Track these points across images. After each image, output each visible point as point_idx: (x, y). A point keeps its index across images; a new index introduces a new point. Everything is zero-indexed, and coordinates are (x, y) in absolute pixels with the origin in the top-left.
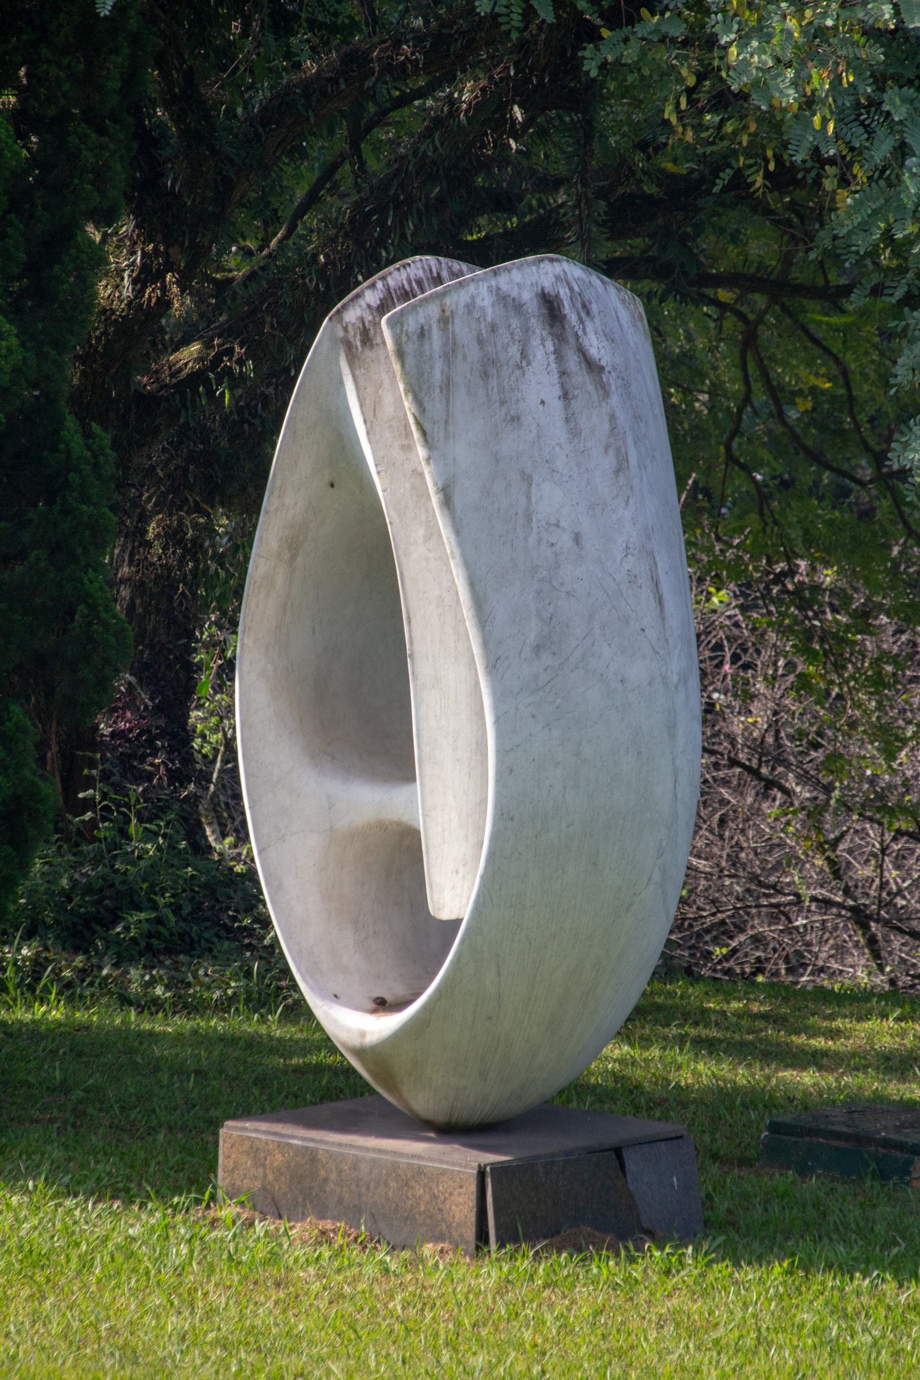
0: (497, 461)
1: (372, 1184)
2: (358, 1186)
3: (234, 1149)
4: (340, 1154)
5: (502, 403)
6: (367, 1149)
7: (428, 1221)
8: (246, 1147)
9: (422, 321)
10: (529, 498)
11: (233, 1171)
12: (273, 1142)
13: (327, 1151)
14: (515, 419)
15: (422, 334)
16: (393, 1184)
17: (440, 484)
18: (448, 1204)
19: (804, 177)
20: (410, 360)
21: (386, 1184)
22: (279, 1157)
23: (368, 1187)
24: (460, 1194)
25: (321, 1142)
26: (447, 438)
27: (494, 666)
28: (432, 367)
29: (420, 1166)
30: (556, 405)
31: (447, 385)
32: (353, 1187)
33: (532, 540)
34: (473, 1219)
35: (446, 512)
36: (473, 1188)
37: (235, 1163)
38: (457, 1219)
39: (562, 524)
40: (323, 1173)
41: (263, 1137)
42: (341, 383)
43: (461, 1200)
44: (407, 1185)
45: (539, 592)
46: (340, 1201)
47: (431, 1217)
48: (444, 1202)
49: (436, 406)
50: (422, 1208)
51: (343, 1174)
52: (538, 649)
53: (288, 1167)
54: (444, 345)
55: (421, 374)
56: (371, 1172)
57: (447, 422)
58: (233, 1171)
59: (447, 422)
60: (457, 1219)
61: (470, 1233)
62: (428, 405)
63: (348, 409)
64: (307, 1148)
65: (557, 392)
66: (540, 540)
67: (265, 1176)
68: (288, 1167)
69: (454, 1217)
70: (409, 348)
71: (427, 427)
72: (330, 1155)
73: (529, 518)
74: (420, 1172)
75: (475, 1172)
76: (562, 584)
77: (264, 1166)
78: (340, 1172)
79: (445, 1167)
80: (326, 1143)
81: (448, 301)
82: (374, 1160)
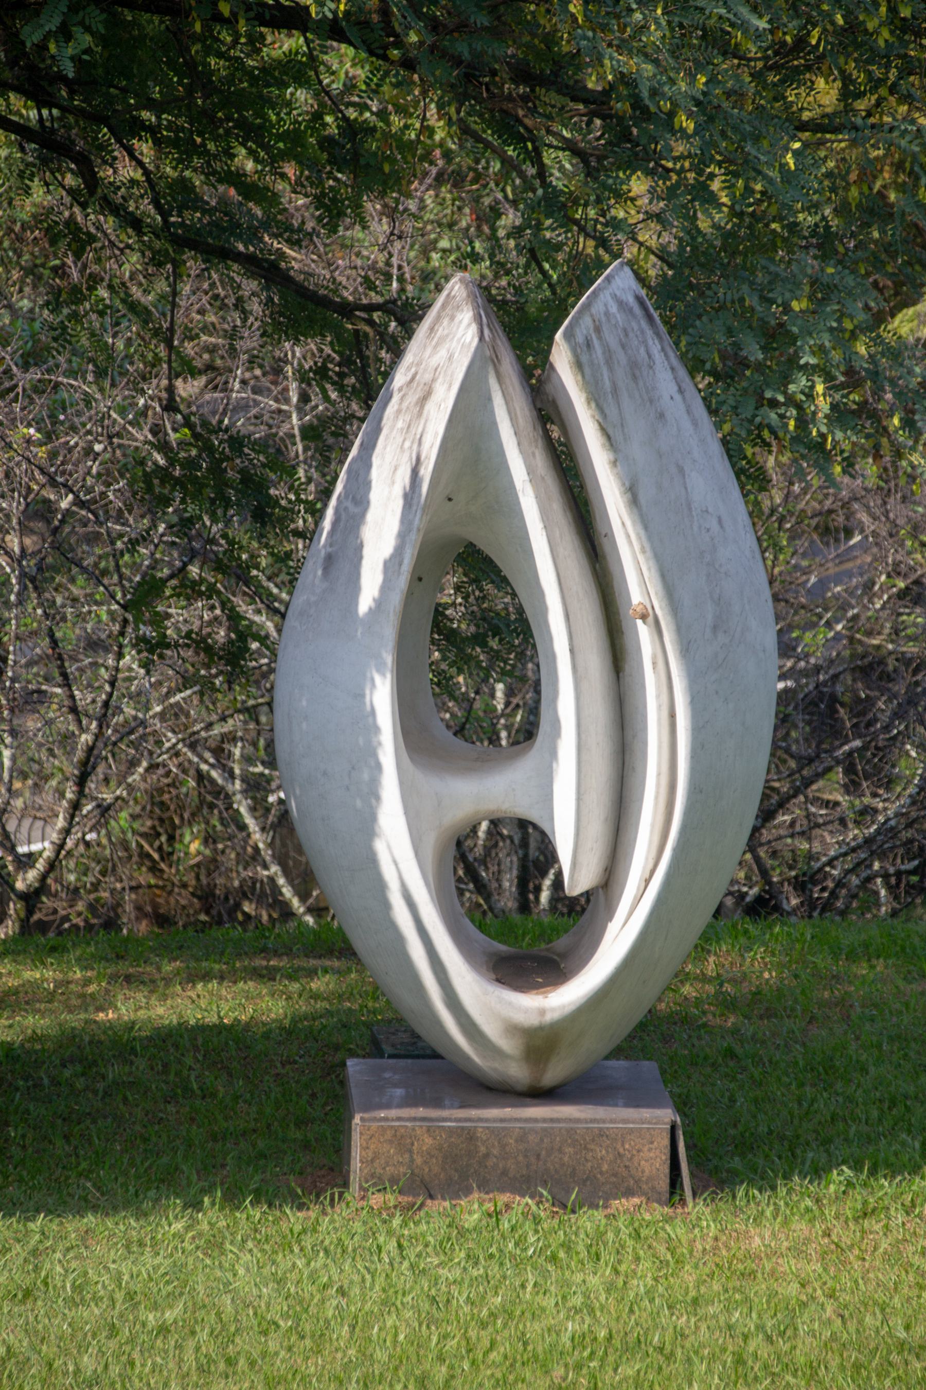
0: (661, 457)
1: (544, 1153)
2: (526, 1156)
3: (373, 1140)
4: (504, 1129)
5: (651, 401)
6: (536, 1120)
7: (614, 1179)
8: (389, 1134)
9: (585, 332)
10: (686, 488)
11: (372, 1161)
12: (421, 1127)
13: (488, 1128)
14: (661, 416)
15: (589, 344)
16: (569, 1150)
17: (627, 484)
18: (636, 1159)
19: (283, 176)
20: (587, 370)
21: (560, 1150)
22: (429, 1141)
23: (538, 1156)
24: (650, 1150)
25: (480, 1120)
26: (625, 439)
27: (687, 650)
28: (602, 375)
29: (600, 1129)
30: (678, 397)
31: (615, 390)
32: (520, 1158)
33: (695, 529)
34: (667, 1171)
35: (635, 510)
36: (666, 1142)
37: (375, 1153)
38: (647, 1173)
39: (710, 510)
40: (483, 1149)
41: (409, 1124)
42: (490, 399)
43: (652, 1155)
44: (586, 1148)
45: (708, 575)
46: (505, 1173)
47: (615, 1175)
48: (631, 1159)
49: (612, 411)
50: (605, 1167)
51: (508, 1149)
52: (715, 628)
53: (440, 1150)
54: (604, 353)
55: (597, 383)
56: (542, 1140)
57: (622, 425)
58: (372, 1161)
59: (622, 425)
60: (647, 1173)
61: (663, 1184)
62: (607, 411)
63: (494, 424)
64: (463, 1128)
65: (676, 388)
66: (700, 527)
67: (412, 1160)
68: (440, 1150)
69: (643, 1172)
70: (584, 358)
71: (611, 433)
72: (492, 1131)
73: (690, 509)
74: (602, 1133)
75: (669, 1127)
76: (721, 566)
77: (411, 1152)
78: (503, 1146)
79: (631, 1126)
80: (487, 1120)
81: (594, 310)
82: (545, 1130)
